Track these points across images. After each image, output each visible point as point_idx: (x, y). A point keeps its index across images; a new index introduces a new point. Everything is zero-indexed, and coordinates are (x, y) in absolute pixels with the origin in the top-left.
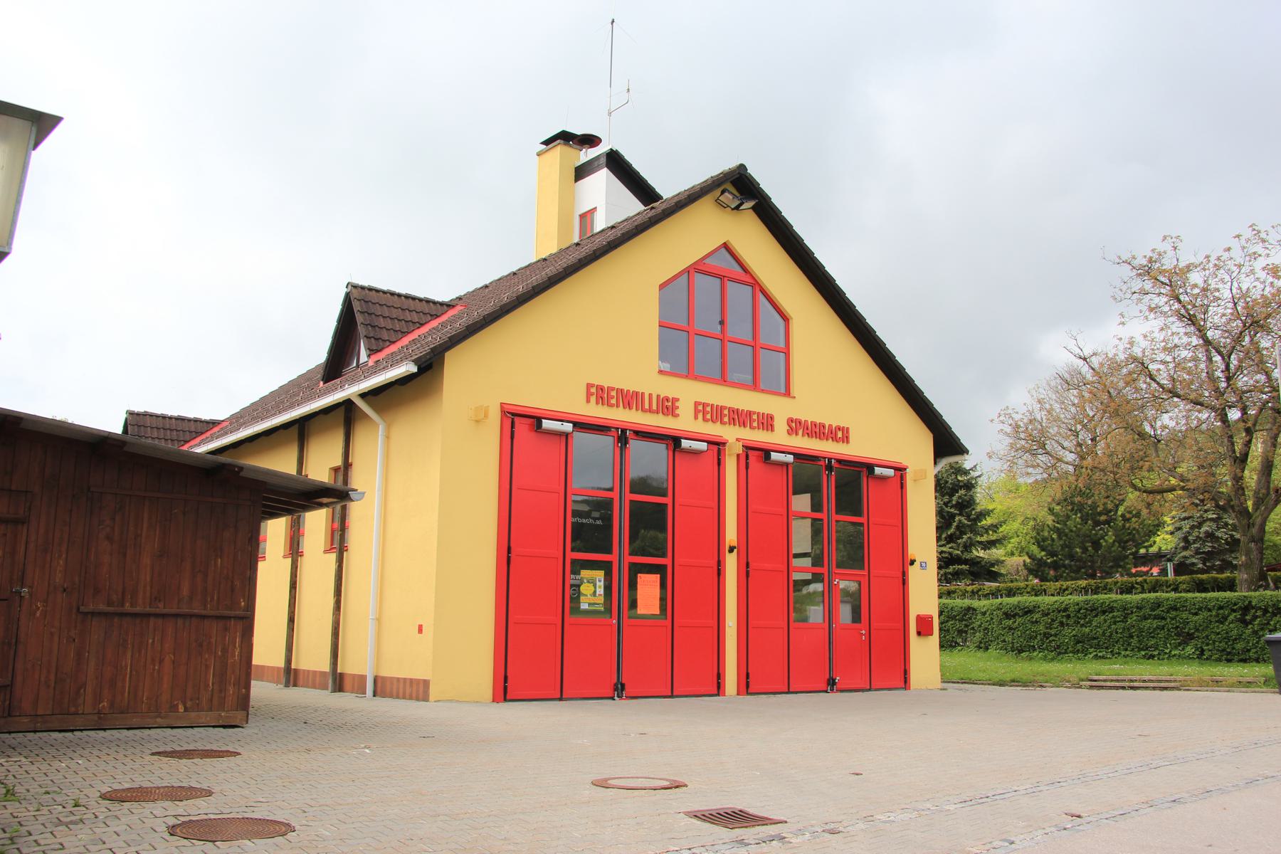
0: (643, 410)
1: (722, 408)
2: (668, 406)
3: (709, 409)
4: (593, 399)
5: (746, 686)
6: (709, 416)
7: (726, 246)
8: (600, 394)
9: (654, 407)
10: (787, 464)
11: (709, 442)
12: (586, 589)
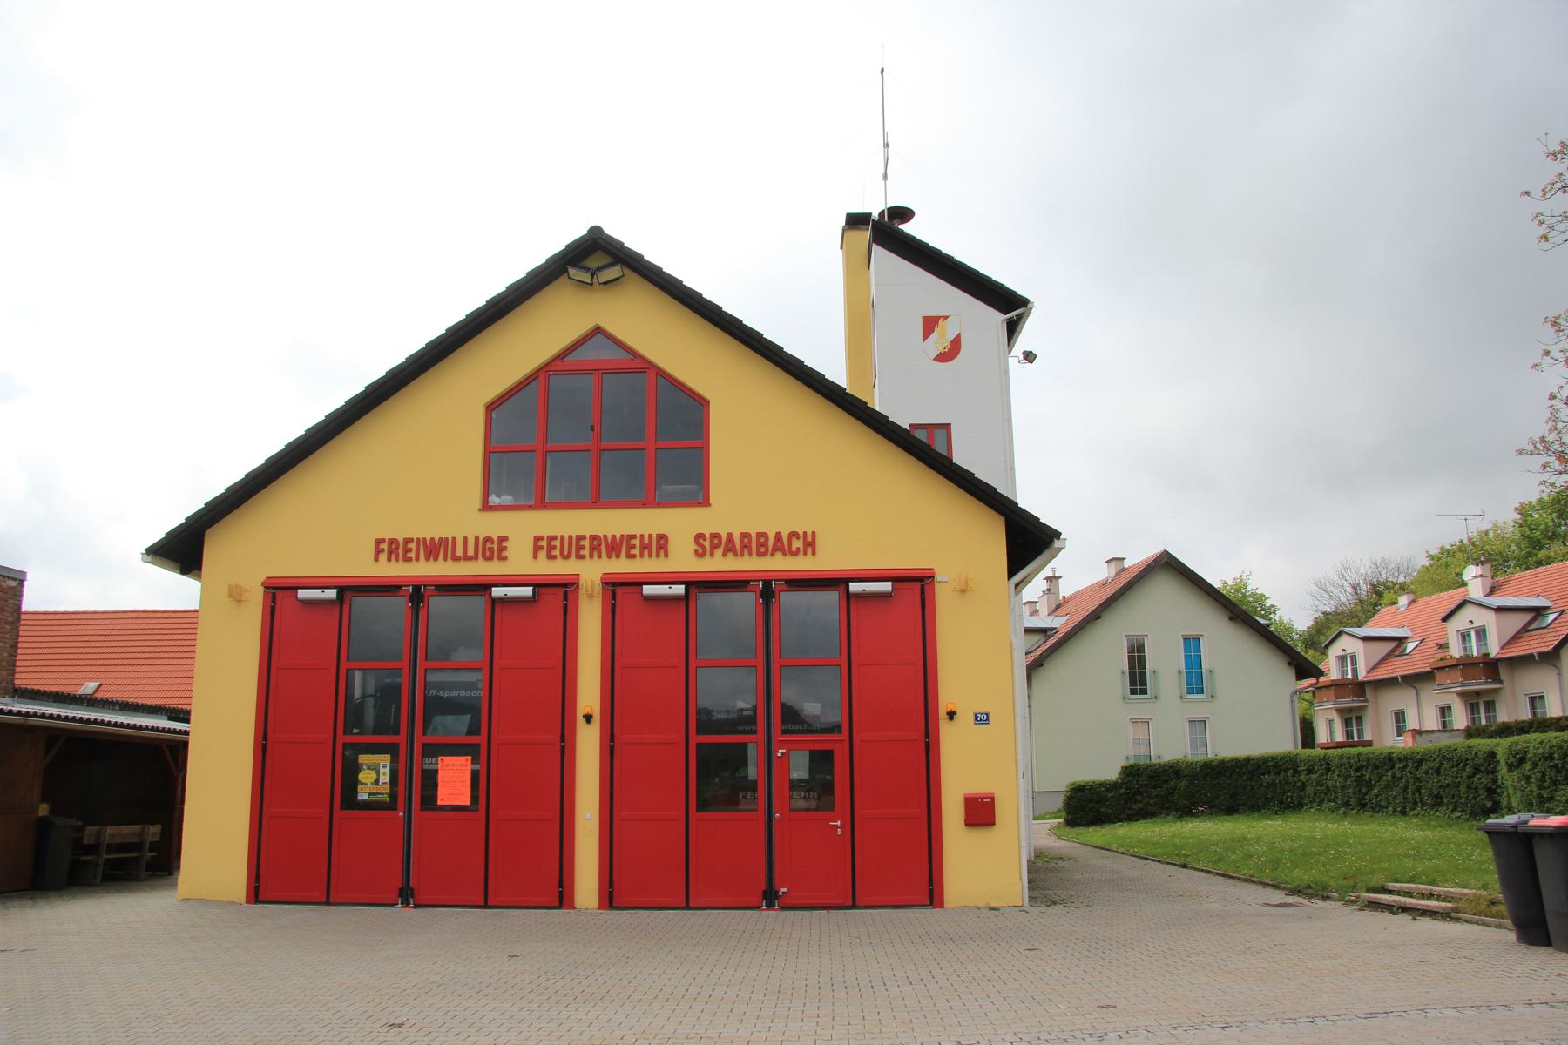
0: (455, 559)
1: (581, 538)
2: (493, 548)
3: (557, 543)
4: (383, 557)
5: (610, 898)
6: (556, 552)
7: (598, 330)
8: (391, 548)
9: (471, 552)
10: (676, 598)
11: (534, 585)
12: (366, 777)
